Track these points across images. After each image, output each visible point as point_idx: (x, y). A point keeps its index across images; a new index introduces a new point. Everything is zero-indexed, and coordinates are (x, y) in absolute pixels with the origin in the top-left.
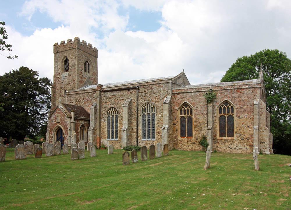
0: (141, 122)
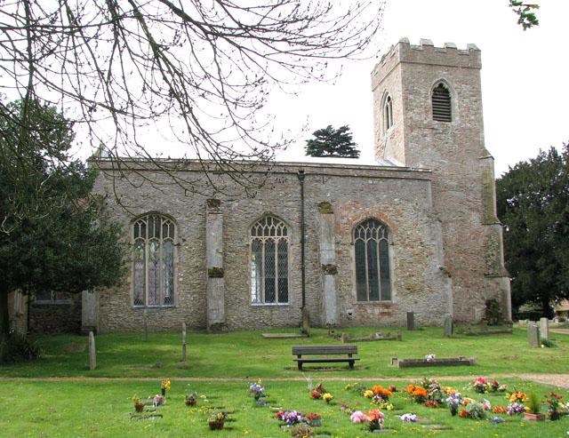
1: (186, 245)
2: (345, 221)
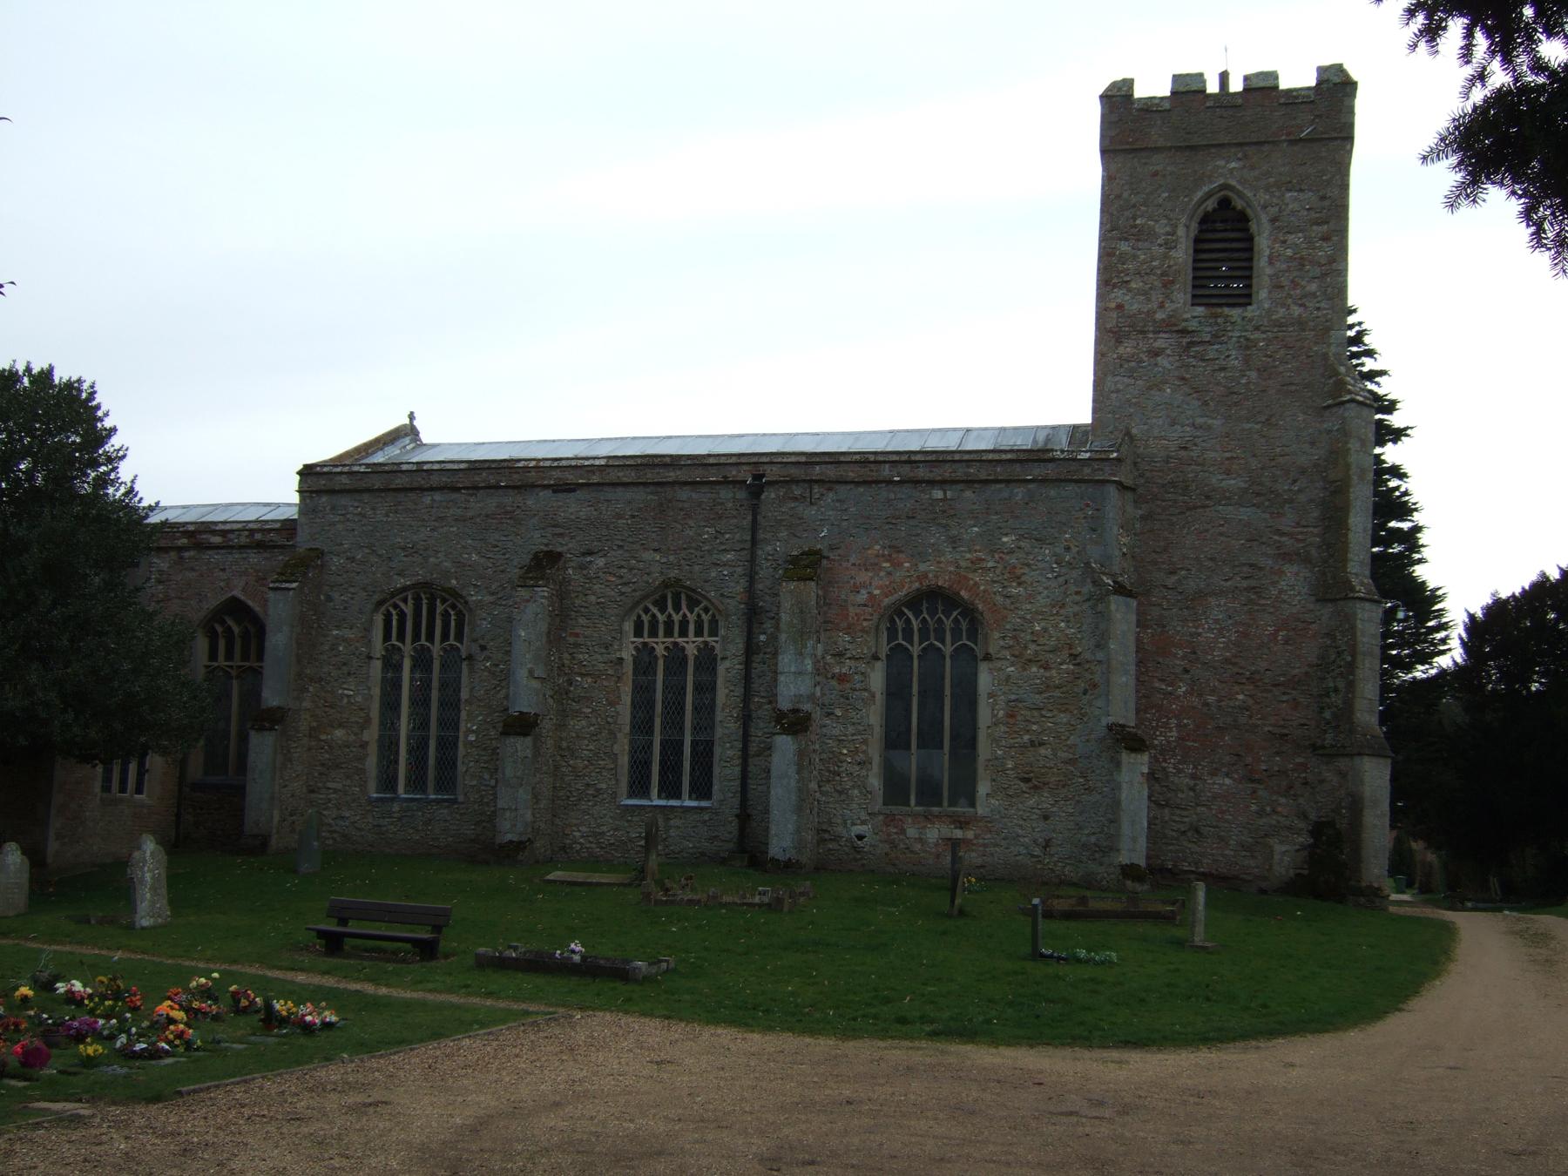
0: (878, 697)
1: (488, 658)
2: (863, 596)
